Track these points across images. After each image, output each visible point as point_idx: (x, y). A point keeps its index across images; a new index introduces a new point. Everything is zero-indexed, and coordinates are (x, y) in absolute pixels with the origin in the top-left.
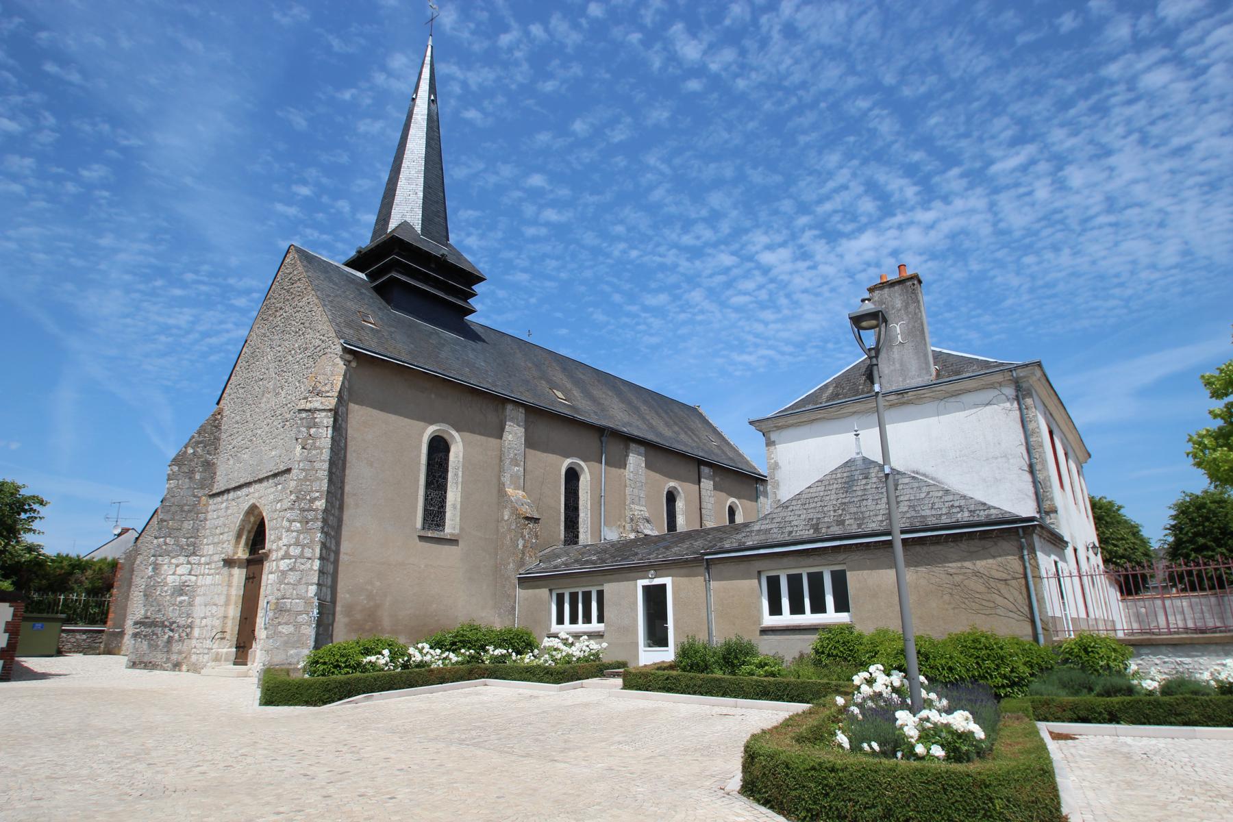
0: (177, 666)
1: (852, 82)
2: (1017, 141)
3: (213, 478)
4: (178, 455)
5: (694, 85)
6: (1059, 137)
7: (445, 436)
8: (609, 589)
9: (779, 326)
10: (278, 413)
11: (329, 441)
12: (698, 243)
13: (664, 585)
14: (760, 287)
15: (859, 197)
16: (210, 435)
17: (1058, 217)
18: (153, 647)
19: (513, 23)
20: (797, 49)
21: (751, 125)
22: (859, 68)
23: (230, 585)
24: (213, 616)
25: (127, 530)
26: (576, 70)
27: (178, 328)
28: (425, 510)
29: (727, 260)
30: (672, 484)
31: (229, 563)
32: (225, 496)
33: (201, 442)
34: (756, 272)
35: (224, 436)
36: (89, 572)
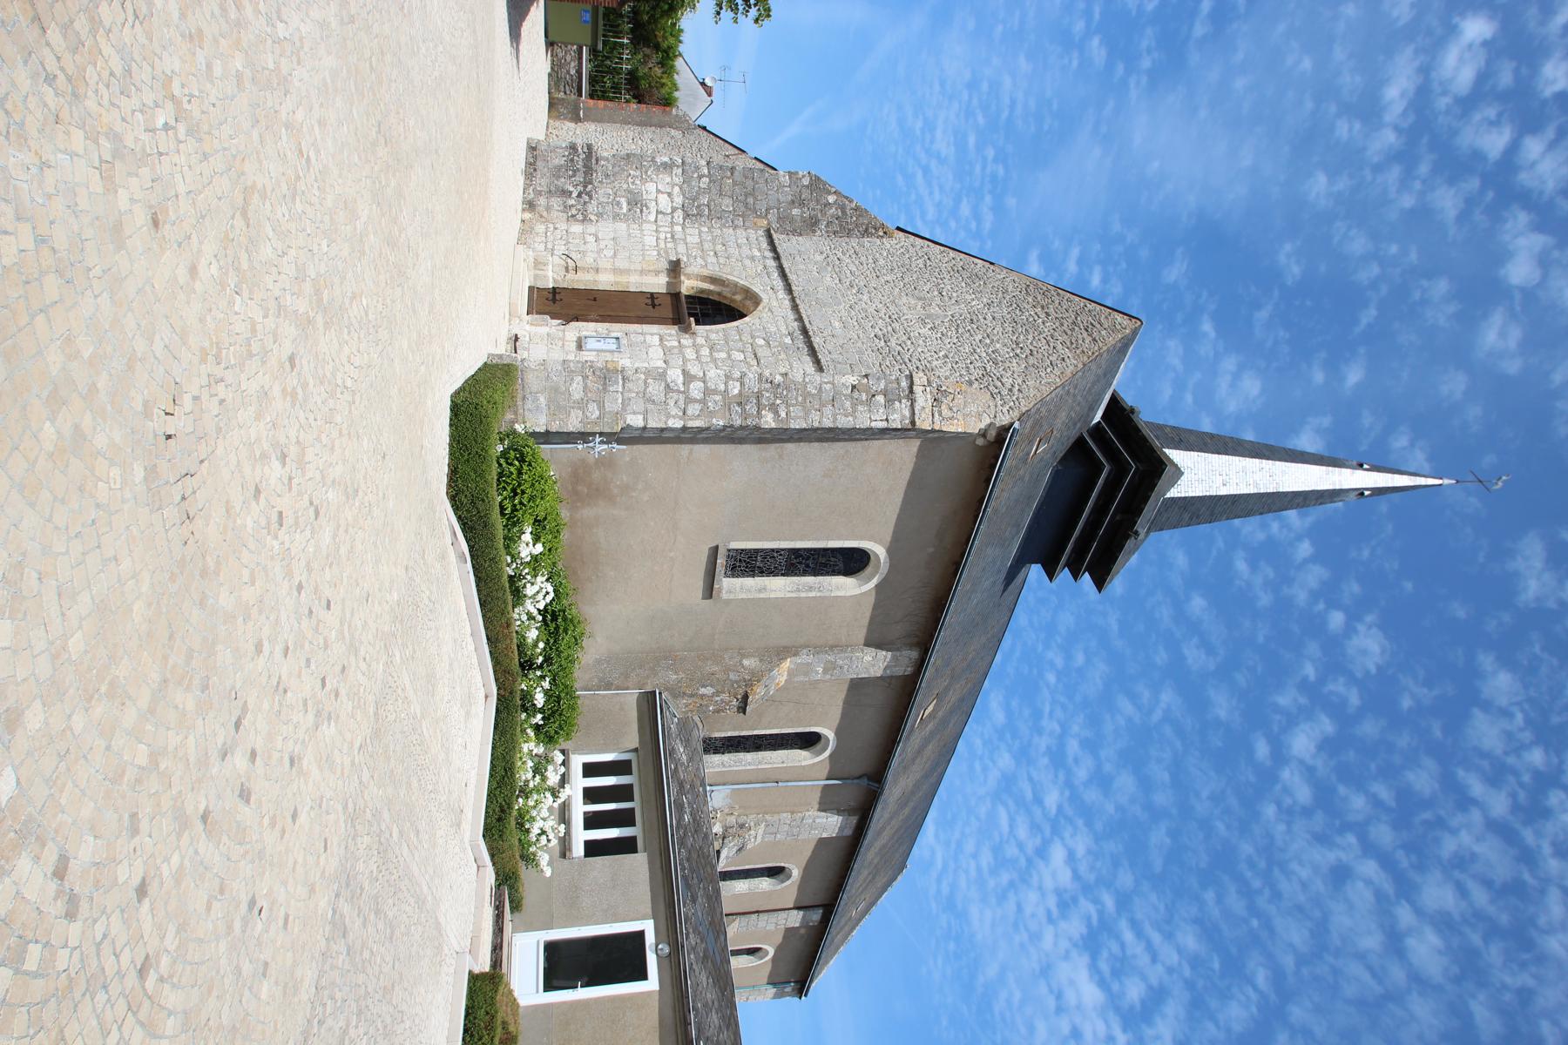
0: (530, 205)
1: (1288, 962)
3: (794, 232)
4: (825, 184)
5: (1262, 749)
7: (869, 570)
8: (637, 865)
9: (973, 873)
10: (895, 325)
11: (866, 424)
12: (1070, 760)
13: (643, 975)
14: (1020, 846)
15: (1144, 978)
16: (856, 223)
18: (557, 172)
19: (1310, 520)
20: (1319, 886)
21: (1220, 826)
22: (1305, 971)
23: (642, 272)
24: (600, 251)
25: (710, 95)
26: (1265, 600)
27: (932, 142)
28: (757, 551)
29: (1052, 799)
30: (796, 873)
31: (675, 268)
32: (769, 254)
33: (844, 212)
34: (1038, 841)
35: (854, 242)
36: (658, 71)
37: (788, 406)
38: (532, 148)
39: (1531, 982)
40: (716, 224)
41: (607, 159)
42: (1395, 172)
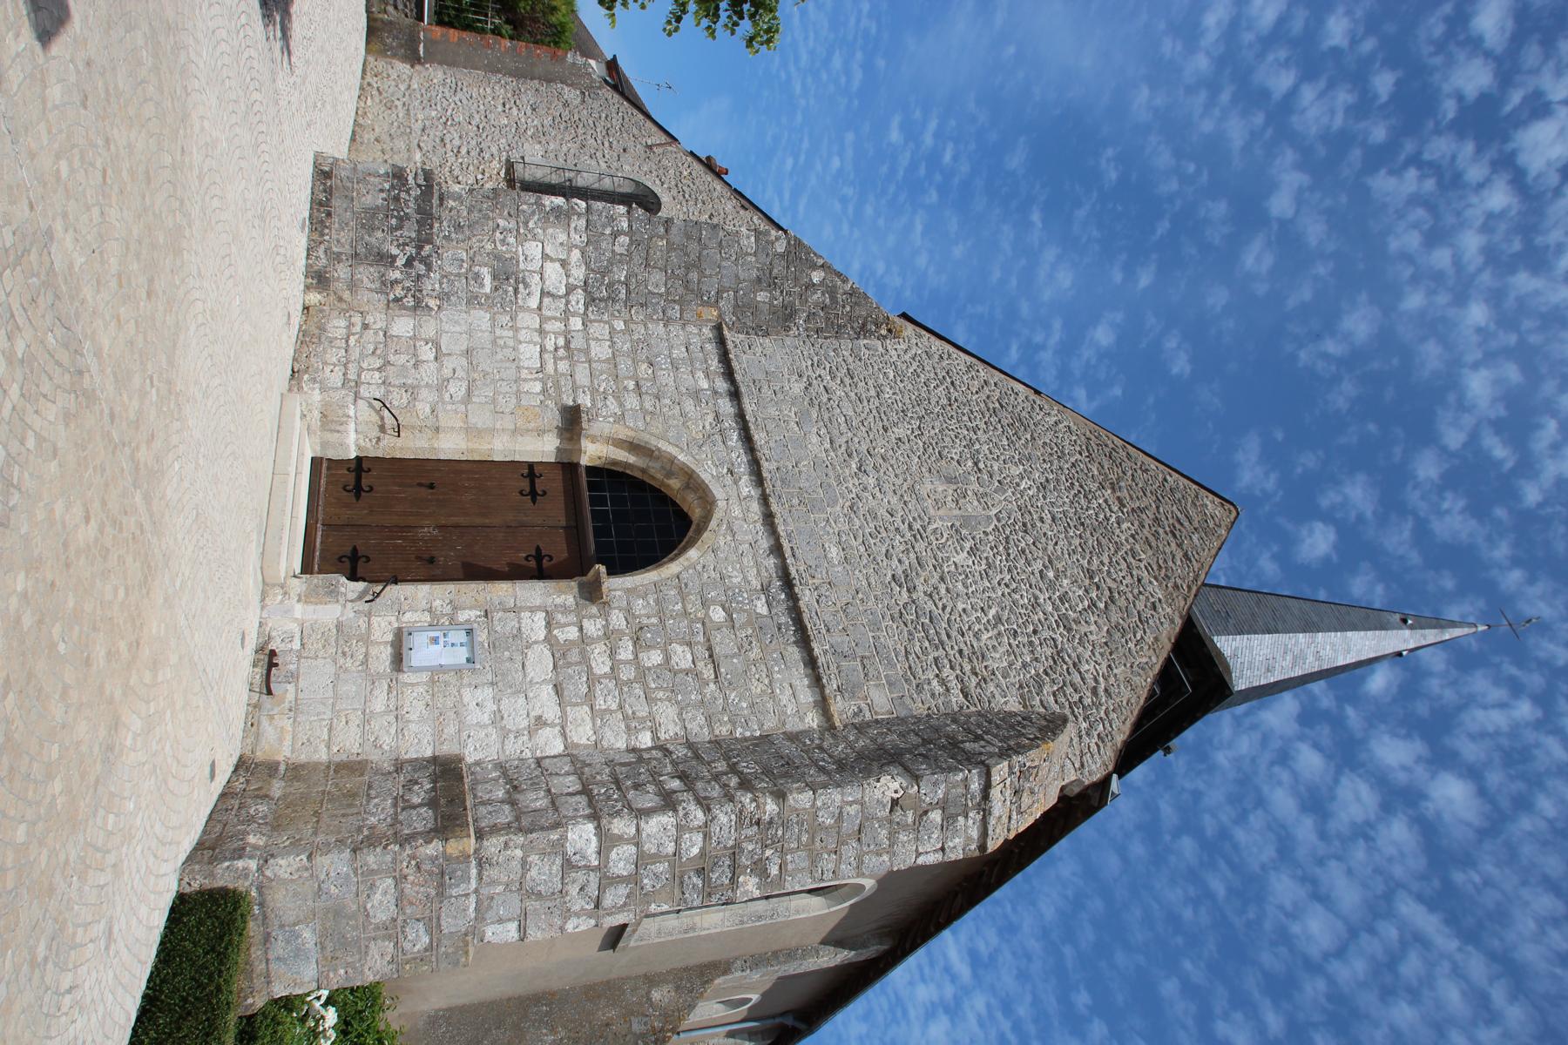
0: (319, 279)
2: (974, 958)
4: (808, 251)
6: (979, 1002)
17: (899, 1014)
18: (369, 220)
31: (572, 421)
32: (722, 385)
33: (833, 298)
35: (846, 344)
37: (782, 852)
38: (323, 174)
39: (1201, 786)
40: (638, 315)
41: (458, 198)
42: (1202, 96)
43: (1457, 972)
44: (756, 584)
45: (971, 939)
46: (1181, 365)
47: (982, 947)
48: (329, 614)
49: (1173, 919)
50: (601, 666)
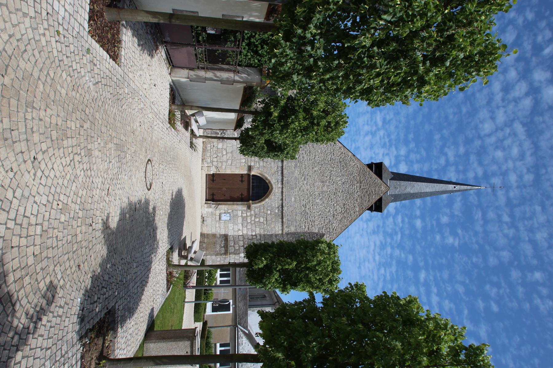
2: (384, 121)
6: (382, 133)
43: (520, 145)
44: (277, 206)
45: (385, 115)
46: (416, 90)
47: (388, 118)
48: (210, 210)
49: (446, 117)
50: (249, 221)
